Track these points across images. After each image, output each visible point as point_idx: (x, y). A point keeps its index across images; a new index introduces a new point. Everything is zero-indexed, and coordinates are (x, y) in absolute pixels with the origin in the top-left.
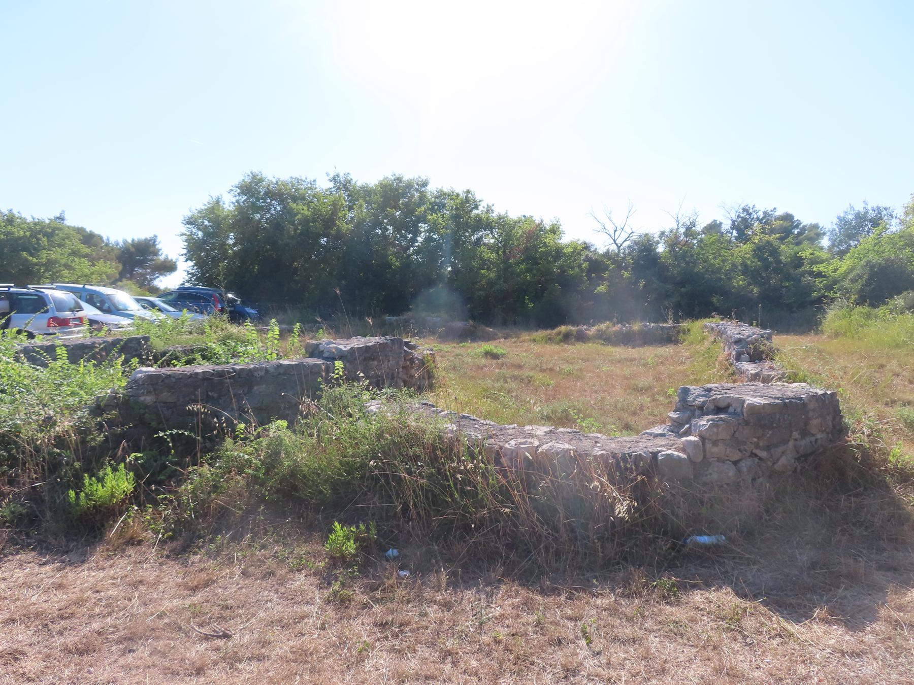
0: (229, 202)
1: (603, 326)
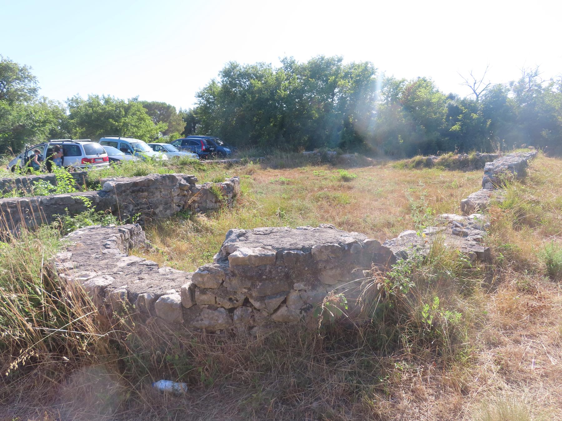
0: (219, 81)
1: (446, 156)
